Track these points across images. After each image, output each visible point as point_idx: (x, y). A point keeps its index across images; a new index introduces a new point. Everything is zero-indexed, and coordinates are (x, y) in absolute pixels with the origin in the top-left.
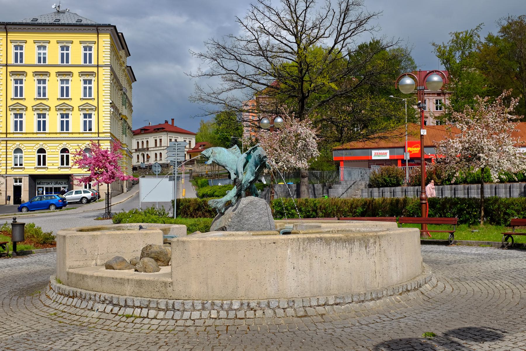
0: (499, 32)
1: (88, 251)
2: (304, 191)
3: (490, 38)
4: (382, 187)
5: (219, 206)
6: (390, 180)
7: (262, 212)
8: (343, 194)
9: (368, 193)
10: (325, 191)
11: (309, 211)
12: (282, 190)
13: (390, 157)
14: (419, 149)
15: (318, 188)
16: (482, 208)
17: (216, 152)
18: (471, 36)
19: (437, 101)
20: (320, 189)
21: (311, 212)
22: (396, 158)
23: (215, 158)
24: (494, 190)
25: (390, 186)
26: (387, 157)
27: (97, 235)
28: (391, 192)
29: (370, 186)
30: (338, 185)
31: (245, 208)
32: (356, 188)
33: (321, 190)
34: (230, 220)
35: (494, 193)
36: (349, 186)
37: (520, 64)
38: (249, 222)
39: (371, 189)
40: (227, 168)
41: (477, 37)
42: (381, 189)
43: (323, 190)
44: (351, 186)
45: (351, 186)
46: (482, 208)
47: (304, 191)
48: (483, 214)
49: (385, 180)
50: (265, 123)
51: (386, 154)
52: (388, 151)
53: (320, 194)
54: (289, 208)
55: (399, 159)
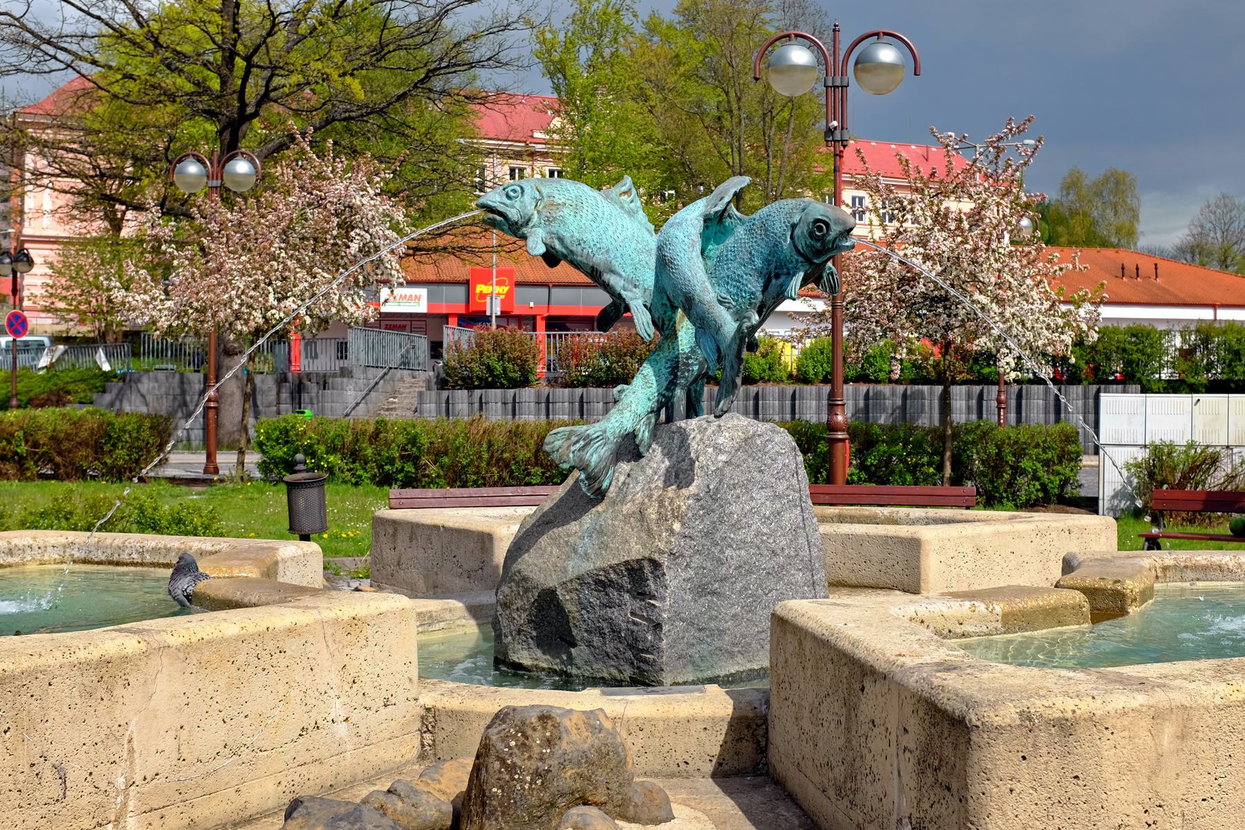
0: (675, 12)
1: (75, 775)
2: (232, 394)
3: (652, 27)
4: (478, 387)
5: (595, 459)
6: (505, 369)
7: (781, 488)
8: (357, 404)
9: (438, 404)
10: (285, 395)
11: (391, 461)
12: (163, 390)
13: (429, 306)
14: (506, 289)
15: (265, 387)
16: (948, 454)
17: (559, 199)
18: (617, 12)
19: (512, 170)
20: (270, 389)
21: (398, 464)
22: (444, 311)
23: (555, 227)
24: (788, 403)
25: (502, 386)
26: (422, 308)
27: (125, 659)
28: (505, 403)
29: (443, 384)
30: (345, 380)
31: (727, 470)
32: (389, 389)
33: (274, 392)
34: (677, 527)
35: (788, 410)
36: (372, 383)
37: (727, 94)
38: (741, 535)
39: (445, 394)
40: (612, 280)
41: (630, 15)
42: (477, 392)
43: (278, 393)
44: (377, 383)
45: (377, 383)
46: (948, 454)
47: (232, 394)
48: (948, 471)
49: (490, 369)
50: (190, 175)
51: (418, 298)
52: (423, 292)
53: (269, 406)
54: (321, 449)
55: (453, 315)
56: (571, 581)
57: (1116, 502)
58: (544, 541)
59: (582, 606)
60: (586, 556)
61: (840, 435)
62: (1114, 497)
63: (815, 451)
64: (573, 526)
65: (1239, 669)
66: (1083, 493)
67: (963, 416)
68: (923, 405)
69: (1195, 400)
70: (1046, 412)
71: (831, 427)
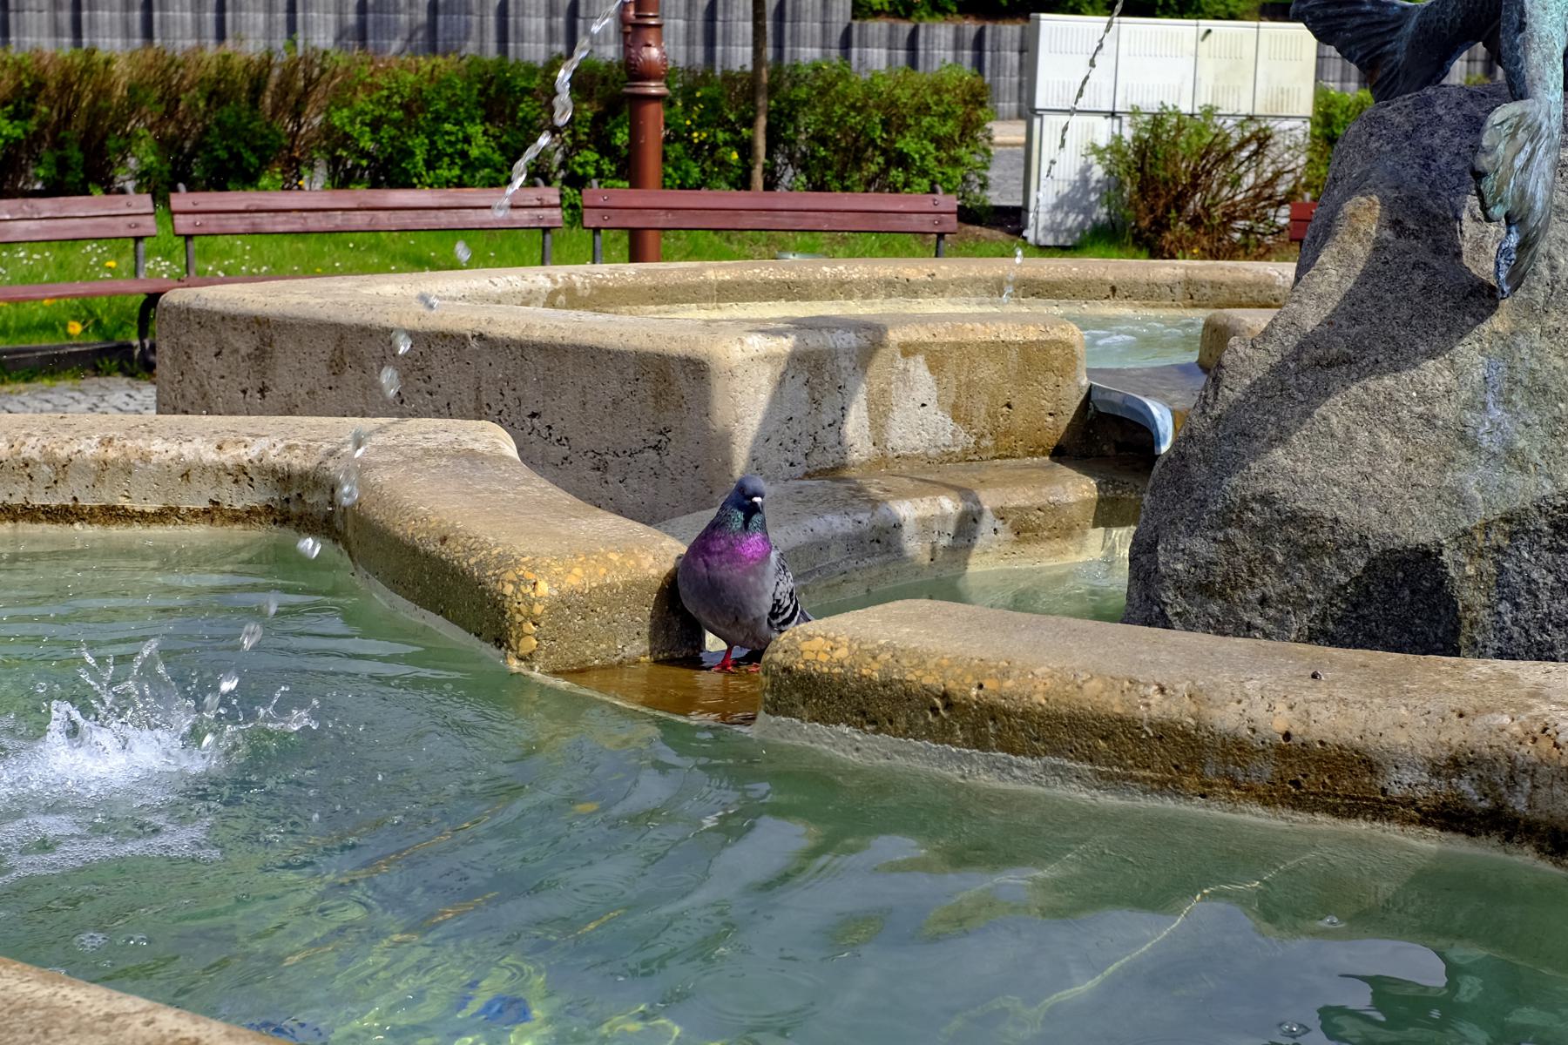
56: (1487, 526)
57: (1059, 217)
58: (1336, 411)
59: (1501, 585)
60: (1513, 457)
61: (654, 88)
62: (1056, 207)
63: (513, 116)
64: (1433, 373)
65: (3, 332)
66: (995, 198)
67: (542, 46)
68: (468, 25)
69: (1203, 29)
70: (689, 42)
71: (635, 71)
